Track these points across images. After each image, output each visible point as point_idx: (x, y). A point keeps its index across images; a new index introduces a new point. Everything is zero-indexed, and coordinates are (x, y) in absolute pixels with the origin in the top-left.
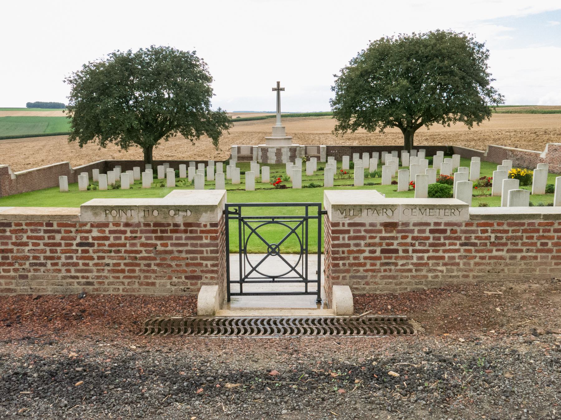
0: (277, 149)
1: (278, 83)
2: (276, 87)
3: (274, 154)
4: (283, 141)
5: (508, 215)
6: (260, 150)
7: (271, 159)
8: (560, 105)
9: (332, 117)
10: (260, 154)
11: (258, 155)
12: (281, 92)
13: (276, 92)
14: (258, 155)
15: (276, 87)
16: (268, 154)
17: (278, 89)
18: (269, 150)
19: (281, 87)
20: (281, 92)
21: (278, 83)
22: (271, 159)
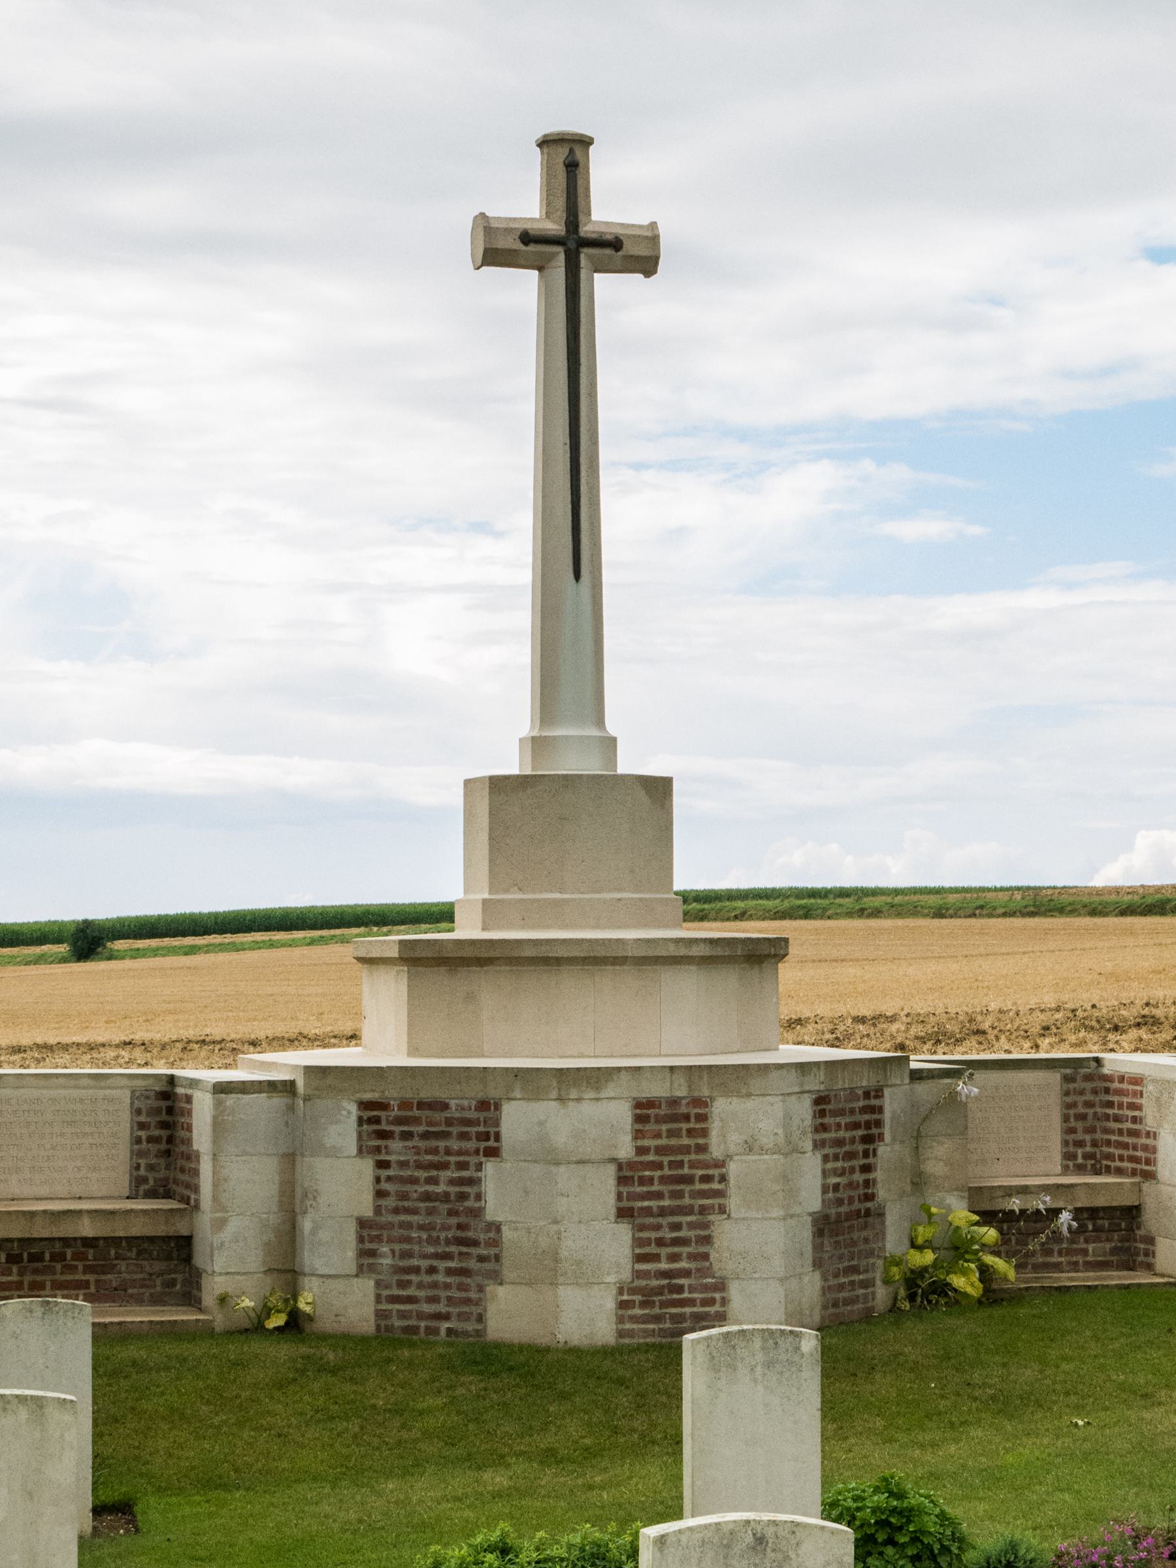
0: (644, 1111)
1: (567, 157)
2: (525, 202)
3: (603, 1189)
4: (684, 985)
5: (336, 1067)
6: (342, 1129)
7: (549, 1269)
8: (9, 972)
9: (63, 949)
10: (344, 1183)
11: (291, 1204)
12: (608, 290)
13: (522, 291)
14: (291, 1204)
15: (525, 202)
16: (499, 1192)
17: (569, 248)
18: (517, 1120)
19: (607, 209)
20: (608, 290)
21: (567, 157)
22: (549, 1269)
